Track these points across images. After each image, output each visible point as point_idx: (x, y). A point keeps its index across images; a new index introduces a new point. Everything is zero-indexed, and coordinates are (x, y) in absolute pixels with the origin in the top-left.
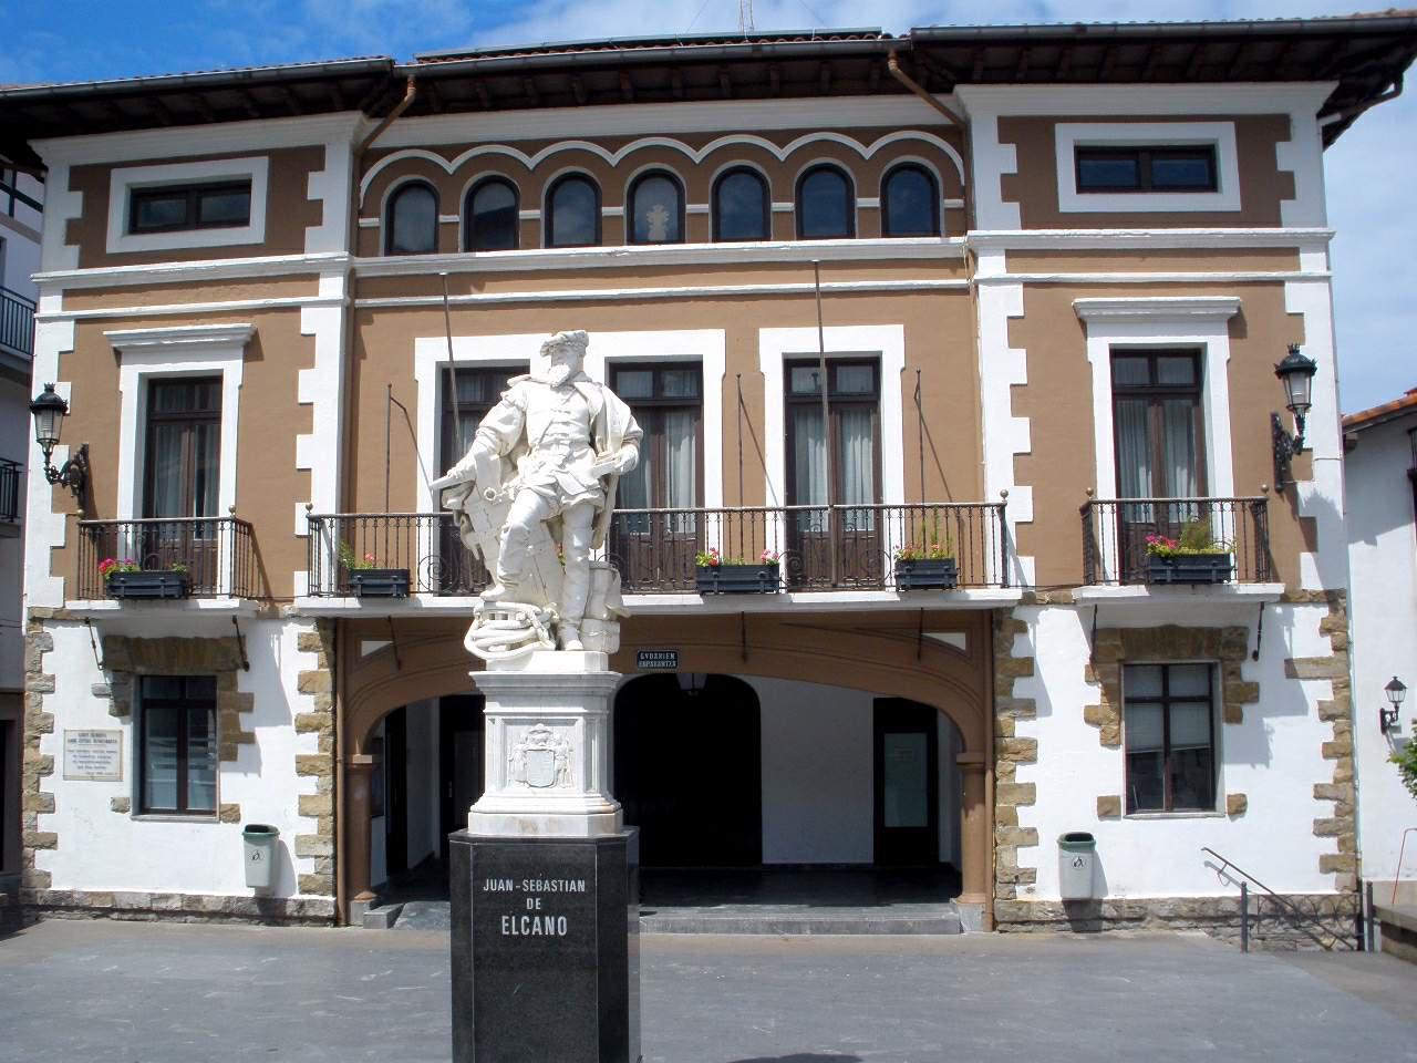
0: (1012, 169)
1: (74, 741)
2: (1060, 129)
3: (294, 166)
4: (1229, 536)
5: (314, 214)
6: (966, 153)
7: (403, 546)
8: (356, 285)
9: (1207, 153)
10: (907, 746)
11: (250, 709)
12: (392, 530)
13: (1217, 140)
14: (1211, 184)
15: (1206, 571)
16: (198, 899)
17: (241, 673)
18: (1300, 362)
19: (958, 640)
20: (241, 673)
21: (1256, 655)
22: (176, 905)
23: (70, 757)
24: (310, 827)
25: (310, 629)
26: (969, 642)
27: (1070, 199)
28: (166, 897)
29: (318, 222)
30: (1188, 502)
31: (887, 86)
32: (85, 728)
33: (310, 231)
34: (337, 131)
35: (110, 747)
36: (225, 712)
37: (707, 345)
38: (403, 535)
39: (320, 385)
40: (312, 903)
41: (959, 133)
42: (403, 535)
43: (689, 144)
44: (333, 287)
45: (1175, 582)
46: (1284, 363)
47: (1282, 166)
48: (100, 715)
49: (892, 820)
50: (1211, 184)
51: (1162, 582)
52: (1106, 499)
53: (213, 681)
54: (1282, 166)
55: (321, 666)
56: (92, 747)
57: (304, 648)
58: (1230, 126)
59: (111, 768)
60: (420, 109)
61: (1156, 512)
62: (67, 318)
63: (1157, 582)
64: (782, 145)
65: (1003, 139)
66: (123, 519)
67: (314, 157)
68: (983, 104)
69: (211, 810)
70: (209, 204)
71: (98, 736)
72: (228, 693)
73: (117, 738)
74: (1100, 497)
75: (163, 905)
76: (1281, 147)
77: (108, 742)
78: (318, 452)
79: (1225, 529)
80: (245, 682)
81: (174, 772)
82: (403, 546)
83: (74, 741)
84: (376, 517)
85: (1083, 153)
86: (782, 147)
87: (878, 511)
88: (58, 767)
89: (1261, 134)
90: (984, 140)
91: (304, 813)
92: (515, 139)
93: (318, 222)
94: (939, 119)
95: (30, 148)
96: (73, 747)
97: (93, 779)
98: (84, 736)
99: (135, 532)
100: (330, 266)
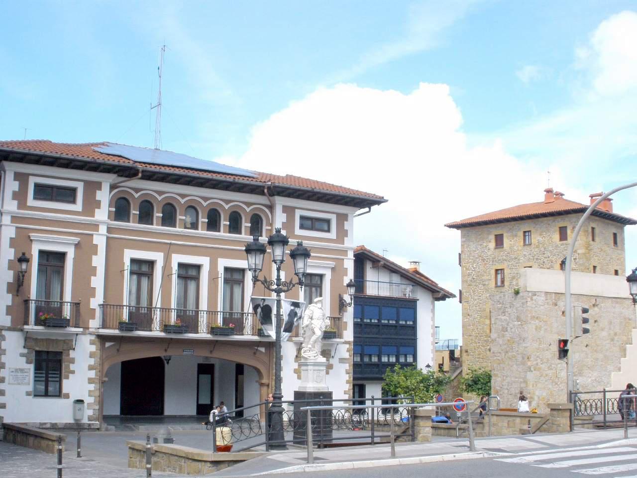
0: (17, 189)
1: (13, 372)
2: (296, 210)
3: (92, 188)
4: (69, 314)
5: (98, 204)
6: (272, 212)
7: (167, 316)
8: (110, 230)
9: (74, 191)
10: (206, 378)
11: (73, 363)
12: (115, 309)
13: (77, 188)
14: (74, 201)
15: (62, 323)
16: (56, 424)
17: (71, 352)
18: (25, 258)
19: (263, 350)
20: (71, 352)
21: (333, 357)
22: (48, 426)
23: (11, 377)
24: (91, 400)
25: (93, 338)
26: (266, 350)
27: (31, 201)
28: (45, 424)
29: (99, 207)
30: (192, 311)
31: (262, 193)
32: (17, 367)
33: (97, 210)
34: (106, 180)
35: (26, 374)
36: (66, 363)
37: (158, 257)
38: (167, 314)
39: (99, 261)
40: (93, 424)
41: (271, 207)
42: (167, 314)
43: (225, 203)
44: (103, 229)
45: (126, 330)
46: (20, 258)
47: (97, 198)
48: (22, 363)
49: (201, 402)
50: (74, 201)
51: (123, 330)
52: (68, 301)
53: (60, 354)
54: (97, 198)
55: (96, 350)
56: (19, 374)
57: (91, 344)
58: (82, 184)
59: (26, 381)
60: (143, 178)
61: (229, 315)
62: (12, 226)
63: (169, 332)
64: (227, 204)
65: (15, 179)
66: (66, 301)
67: (98, 186)
68: (280, 202)
69: (59, 394)
70: (317, 225)
71: (22, 370)
72: (67, 357)
73: (28, 370)
74: (31, 299)
75: (44, 426)
76: (98, 192)
77: (25, 372)
78: (98, 282)
79: (67, 312)
80: (72, 354)
81: (43, 383)
82: (167, 316)
83: (13, 372)
84: (114, 305)
85: (37, 186)
86: (183, 199)
87: (243, 314)
88: (7, 380)
89: (342, 218)
90: (278, 209)
91: (90, 396)
92: (133, 187)
93: (99, 207)
94: (268, 203)
95: (3, 165)
96: (12, 373)
97: (19, 384)
98: (16, 370)
99: (160, 311)
100: (103, 223)
